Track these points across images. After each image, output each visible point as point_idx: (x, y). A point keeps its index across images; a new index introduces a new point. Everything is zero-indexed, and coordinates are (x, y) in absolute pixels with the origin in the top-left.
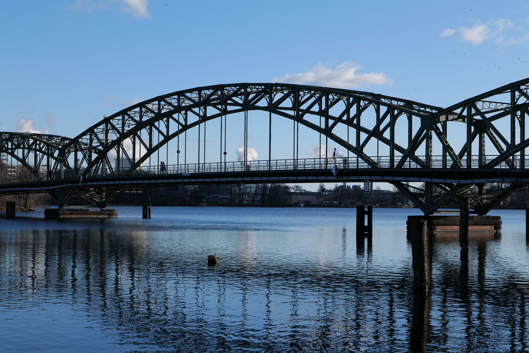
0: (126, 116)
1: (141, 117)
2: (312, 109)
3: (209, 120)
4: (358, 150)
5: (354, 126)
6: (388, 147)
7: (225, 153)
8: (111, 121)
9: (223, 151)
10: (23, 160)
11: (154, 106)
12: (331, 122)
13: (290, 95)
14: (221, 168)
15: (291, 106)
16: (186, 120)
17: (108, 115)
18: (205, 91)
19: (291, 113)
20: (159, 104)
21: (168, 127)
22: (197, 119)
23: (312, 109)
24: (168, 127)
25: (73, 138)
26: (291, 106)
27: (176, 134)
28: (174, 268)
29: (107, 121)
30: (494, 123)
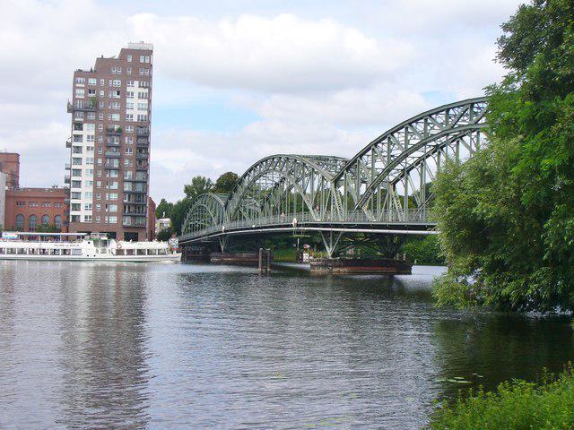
11: (441, 118)
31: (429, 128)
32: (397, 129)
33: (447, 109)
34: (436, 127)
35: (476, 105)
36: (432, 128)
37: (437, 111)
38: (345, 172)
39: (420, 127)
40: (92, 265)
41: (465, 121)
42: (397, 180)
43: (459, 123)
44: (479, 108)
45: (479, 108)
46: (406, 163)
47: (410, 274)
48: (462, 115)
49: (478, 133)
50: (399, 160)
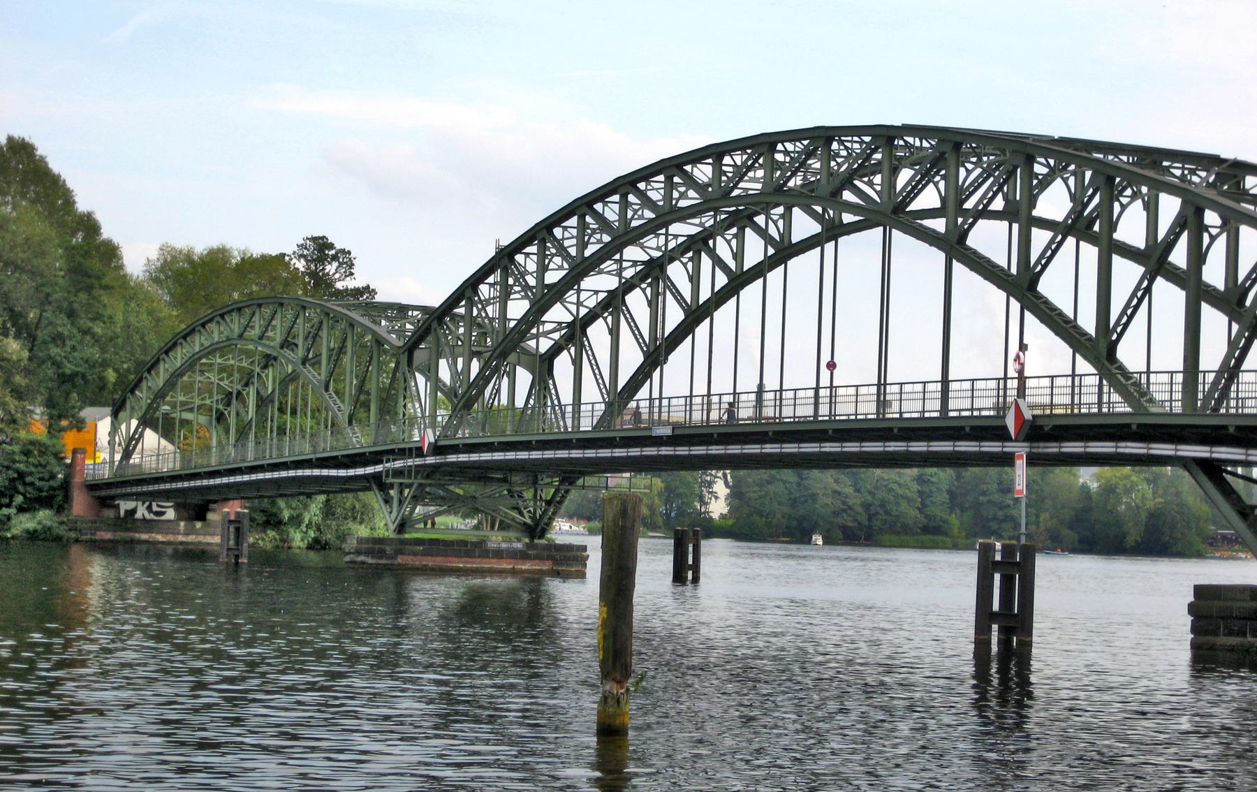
0: (632, 198)
1: (583, 245)
2: (992, 207)
3: (848, 233)
4: (1099, 348)
5: (1093, 239)
6: (1181, 294)
7: (832, 366)
8: (598, 207)
9: (825, 358)
10: (1099, 348)
11: (703, 172)
12: (1040, 238)
13: (683, 254)
14: (660, 412)
15: (936, 203)
16: (738, 256)
17: (505, 242)
18: (787, 144)
19: (939, 225)
20: (625, 204)
21: (694, 279)
22: (815, 228)
23: (992, 207)
24: (694, 279)
25: (437, 305)
26: (936, 203)
27: (760, 271)
28: (561, 751)
29: (504, 258)
30: (1141, 244)
31: (676, 195)
32: (558, 218)
33: (716, 152)
34: (691, 193)
35: (780, 147)
36: (683, 196)
37: (696, 156)
38: (435, 325)
39: (611, 212)
40: (1106, 389)
41: (753, 184)
42: (556, 350)
43: (741, 185)
44: (786, 153)
45: (786, 153)
46: (579, 304)
47: (1200, 591)
48: (749, 168)
49: (789, 209)
50: (555, 294)
